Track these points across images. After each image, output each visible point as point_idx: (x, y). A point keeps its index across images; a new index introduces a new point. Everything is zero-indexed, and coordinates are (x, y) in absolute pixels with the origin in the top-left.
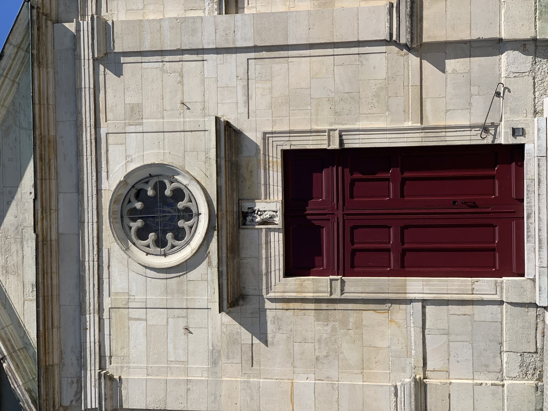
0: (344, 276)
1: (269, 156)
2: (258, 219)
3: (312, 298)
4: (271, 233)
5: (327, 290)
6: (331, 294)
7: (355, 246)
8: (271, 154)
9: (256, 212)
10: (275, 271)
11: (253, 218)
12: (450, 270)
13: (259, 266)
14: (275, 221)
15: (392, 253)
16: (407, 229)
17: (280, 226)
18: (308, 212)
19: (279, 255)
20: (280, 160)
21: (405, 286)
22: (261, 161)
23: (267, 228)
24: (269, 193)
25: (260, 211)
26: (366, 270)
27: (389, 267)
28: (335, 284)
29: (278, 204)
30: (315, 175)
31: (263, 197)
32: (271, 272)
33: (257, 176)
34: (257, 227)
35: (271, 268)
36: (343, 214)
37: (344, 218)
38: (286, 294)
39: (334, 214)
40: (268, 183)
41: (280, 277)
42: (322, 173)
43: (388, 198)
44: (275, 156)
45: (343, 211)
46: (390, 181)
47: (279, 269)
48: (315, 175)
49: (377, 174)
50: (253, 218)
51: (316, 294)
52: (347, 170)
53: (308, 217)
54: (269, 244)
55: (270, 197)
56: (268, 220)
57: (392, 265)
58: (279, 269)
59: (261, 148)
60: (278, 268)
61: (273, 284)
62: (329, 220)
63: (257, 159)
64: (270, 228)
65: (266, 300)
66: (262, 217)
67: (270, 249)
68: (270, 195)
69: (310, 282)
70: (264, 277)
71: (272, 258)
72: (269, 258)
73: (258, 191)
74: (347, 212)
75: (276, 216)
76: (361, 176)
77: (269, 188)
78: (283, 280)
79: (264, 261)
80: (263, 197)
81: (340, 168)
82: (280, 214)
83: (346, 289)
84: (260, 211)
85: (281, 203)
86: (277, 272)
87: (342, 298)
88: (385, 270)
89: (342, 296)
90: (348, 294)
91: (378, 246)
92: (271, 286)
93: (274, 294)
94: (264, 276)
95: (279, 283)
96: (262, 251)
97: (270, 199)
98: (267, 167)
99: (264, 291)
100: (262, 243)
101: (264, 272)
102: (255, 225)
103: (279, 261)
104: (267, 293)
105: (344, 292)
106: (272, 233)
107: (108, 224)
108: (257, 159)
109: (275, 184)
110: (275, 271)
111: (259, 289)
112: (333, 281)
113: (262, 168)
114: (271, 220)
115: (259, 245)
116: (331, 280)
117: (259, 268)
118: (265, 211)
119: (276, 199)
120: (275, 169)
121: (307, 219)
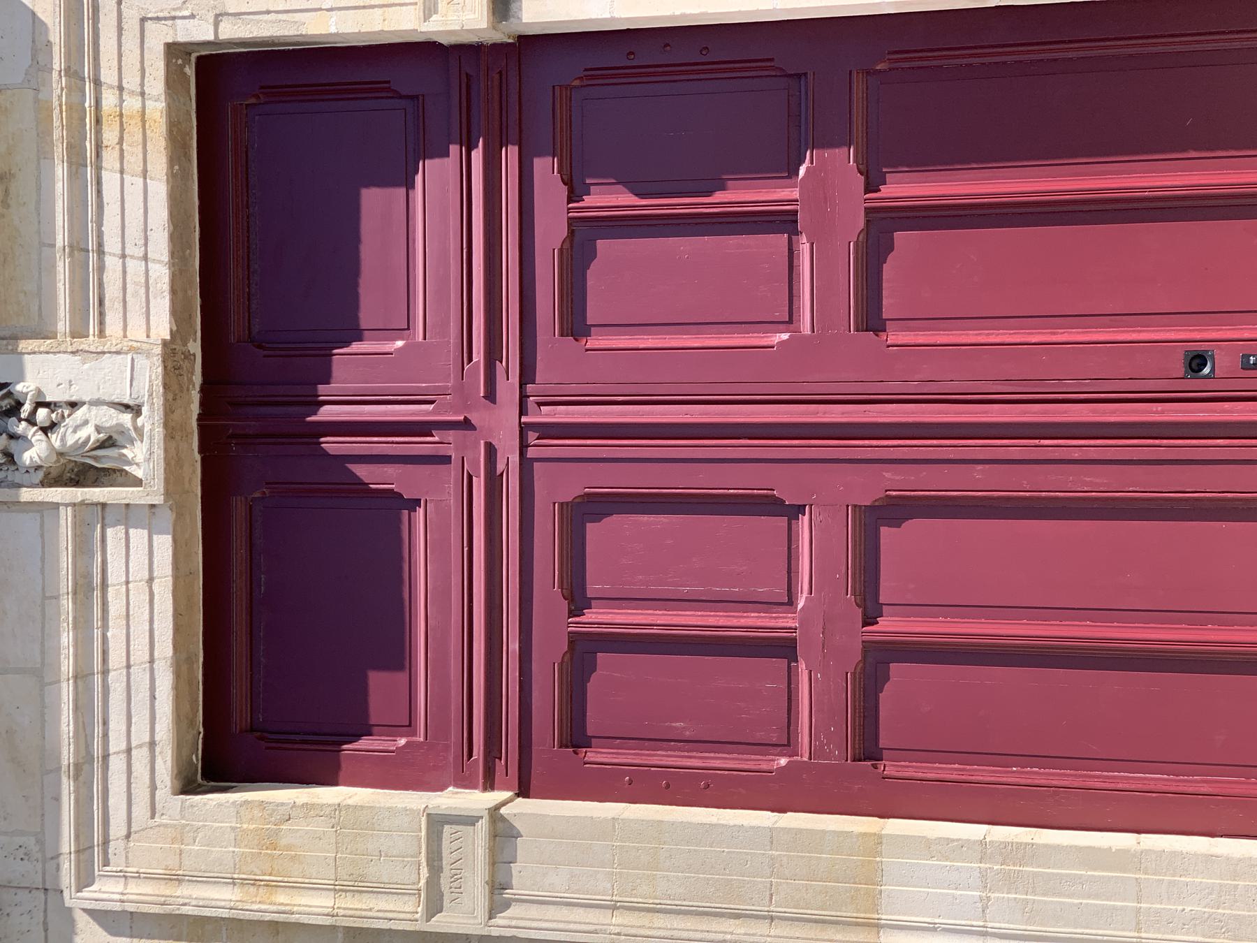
0: (524, 791)
1: (97, 83)
2: (36, 451)
3: (328, 921)
4: (110, 532)
5: (414, 877)
6: (434, 906)
7: (590, 616)
8: (108, 75)
9: (24, 413)
10: (129, 751)
11: (14, 446)
12: (1160, 787)
13: (43, 721)
14: (129, 463)
15: (802, 666)
16: (896, 522)
17: (152, 492)
18: (327, 413)
19: (152, 661)
20: (162, 105)
21: (872, 876)
22: (56, 112)
23: (82, 503)
24: (101, 302)
25: (47, 405)
26: (655, 761)
27: (788, 745)
28: (455, 845)
29: (141, 361)
30: (373, 200)
31: (63, 325)
32: (106, 757)
33: (38, 202)
34: (27, 495)
35: (106, 735)
36: (523, 429)
37: (531, 453)
38: (185, 891)
39: (473, 428)
40: (92, 244)
41: (153, 788)
42: (410, 185)
43: (785, 336)
44: (131, 82)
45: (523, 411)
46: (797, 233)
47: (152, 744)
48: (373, 200)
49: (723, 188)
50: (13, 442)
51: (350, 903)
52: (545, 169)
53: (331, 444)
54: (97, 594)
55: (102, 323)
56: (96, 458)
57: (804, 739)
58: (152, 744)
59: (56, 35)
60: (147, 739)
61: (117, 827)
62: (446, 460)
63: (37, 101)
64: (104, 505)
65: (82, 921)
66: (55, 438)
67: (105, 627)
68: (102, 314)
69: (319, 826)
70: (67, 787)
71: (112, 675)
72: (98, 679)
73: (40, 288)
74: (549, 415)
75: (133, 434)
76: (627, 199)
77: (101, 269)
78: (174, 805)
79: (67, 692)
80: (63, 325)
81: (510, 156)
82: (151, 421)
83: (523, 876)
84: (47, 405)
85: (157, 362)
86: (140, 758)
87: (495, 932)
88: (764, 766)
89: (498, 921)
90: (534, 911)
91: (722, 622)
92: (106, 842)
93: (120, 888)
94: (64, 780)
95: (151, 824)
96: (59, 636)
97: (101, 333)
98: (89, 146)
99: (67, 875)
100: (58, 590)
101: (67, 755)
102: (20, 486)
103: (153, 697)
104: (85, 879)
105: (508, 893)
106: (114, 535)
107: (97, 490)
108: (37, 101)
109: (134, 250)
110: (129, 751)
111: (42, 850)
112: (447, 828)
113: (60, 151)
114: (107, 459)
115: (45, 598)
116: (437, 822)
117: (43, 728)
118: (73, 405)
119: (137, 332)
120: (134, 160)
121: (325, 454)
